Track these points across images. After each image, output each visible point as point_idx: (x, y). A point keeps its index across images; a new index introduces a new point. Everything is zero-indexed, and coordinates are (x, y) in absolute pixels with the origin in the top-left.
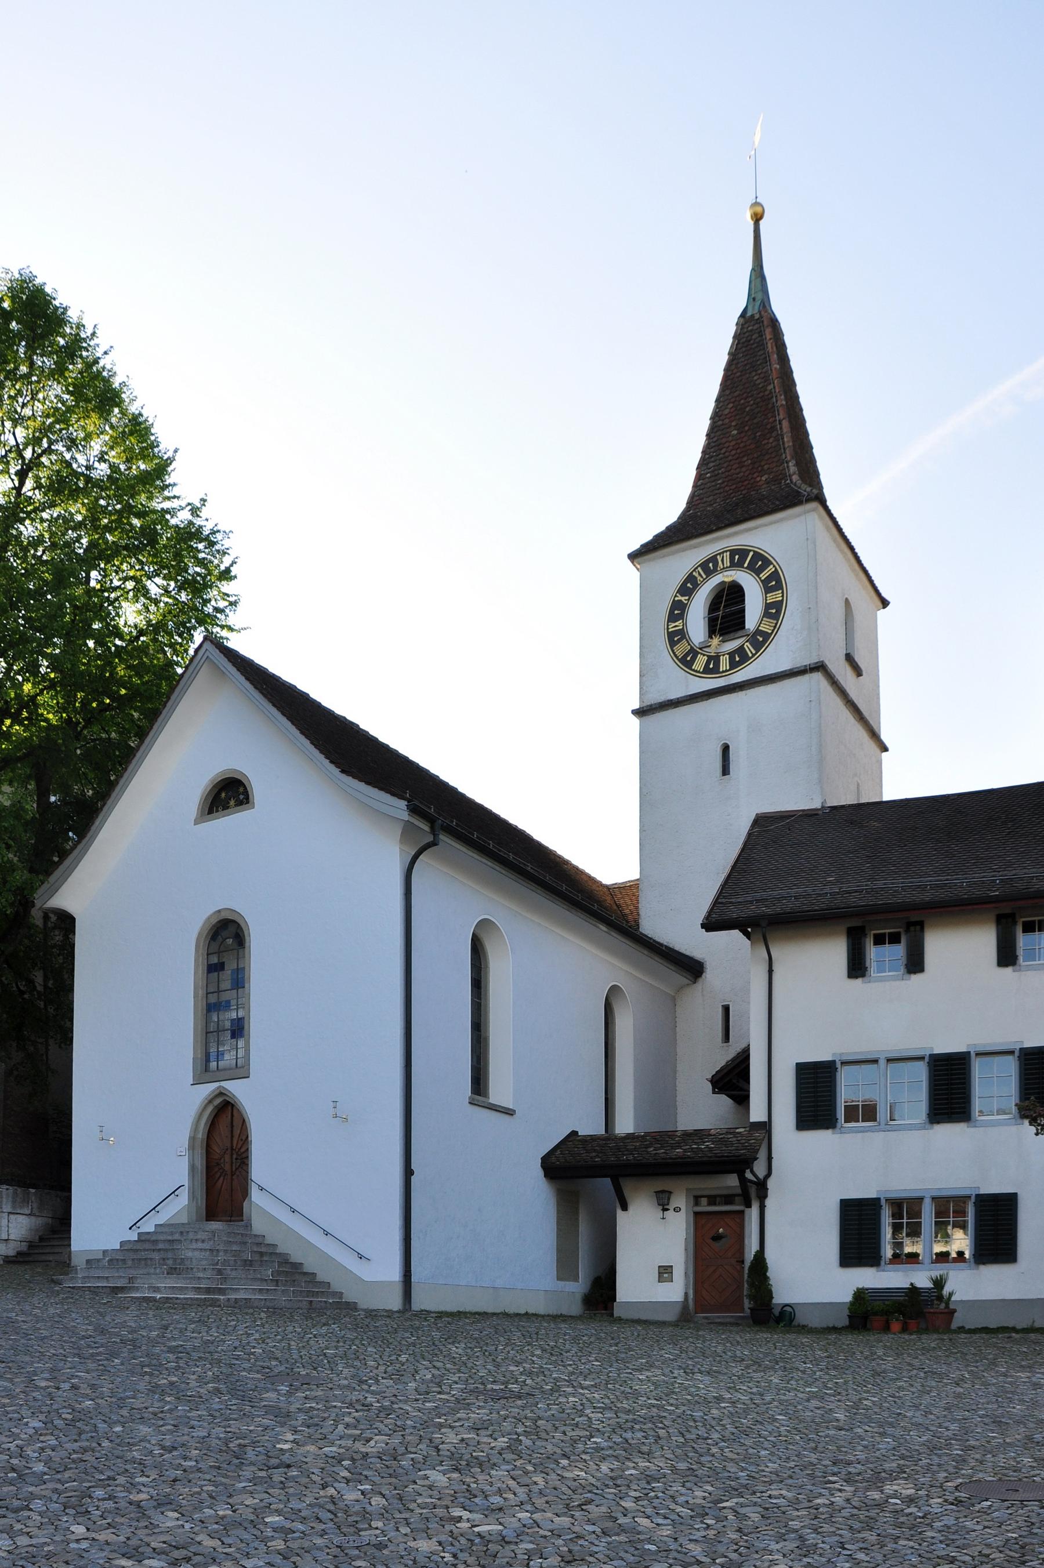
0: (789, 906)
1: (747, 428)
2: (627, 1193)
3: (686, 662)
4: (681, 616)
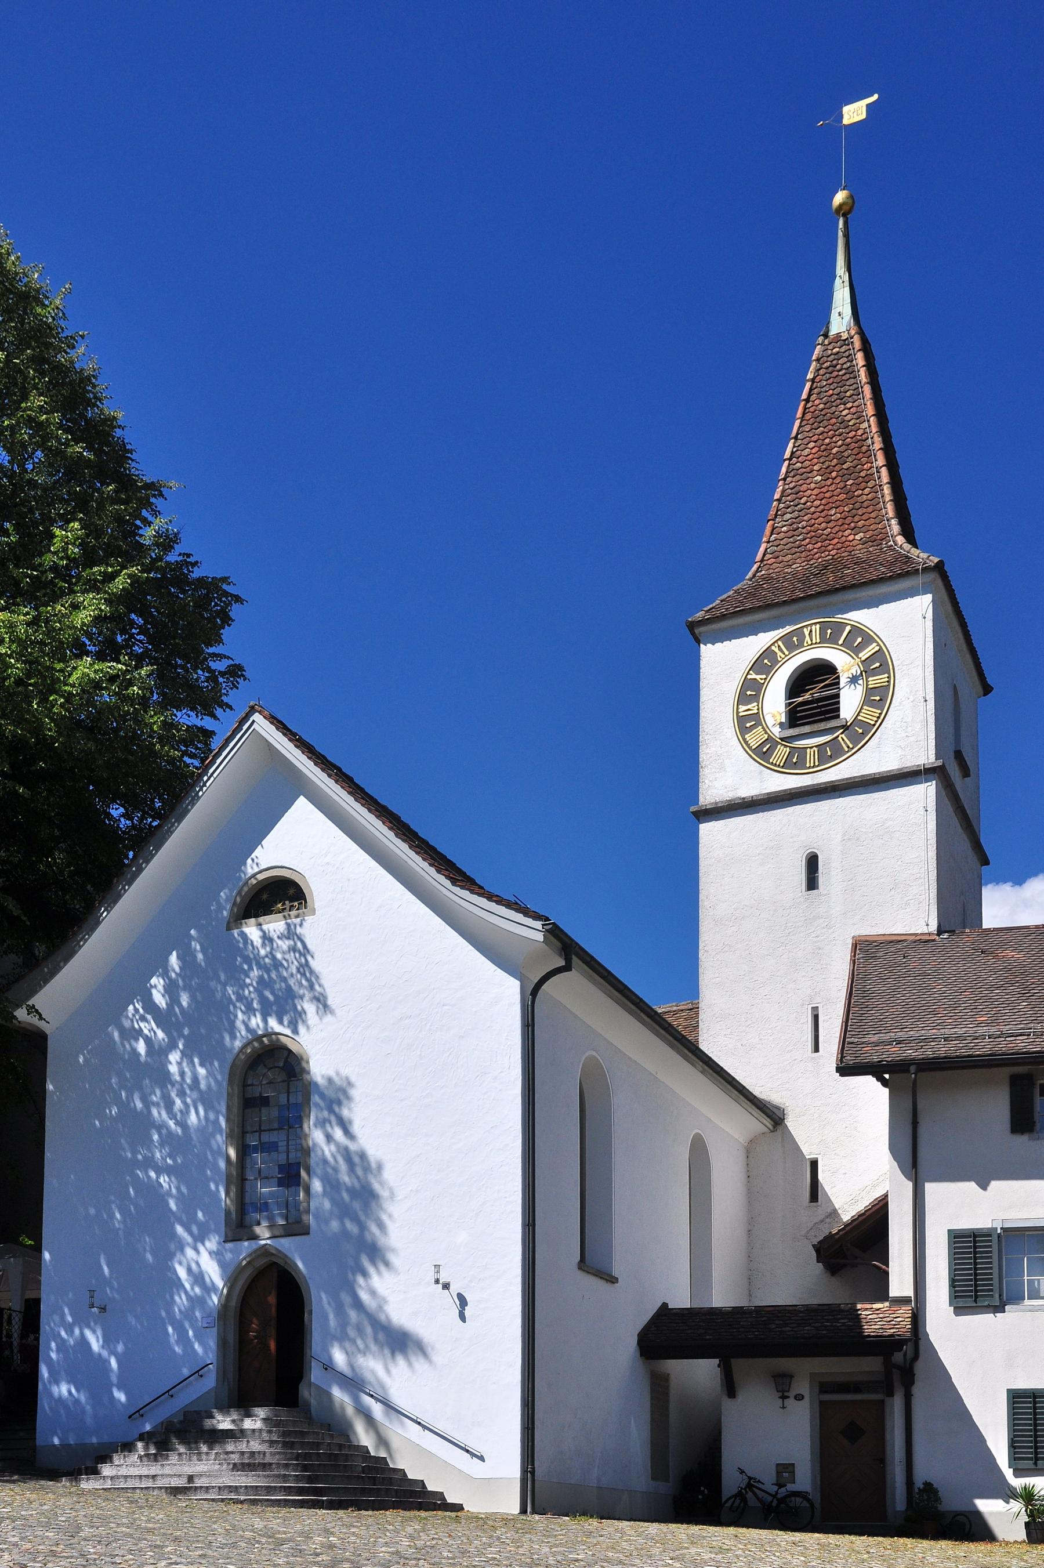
0: (943, 1050)
1: (834, 474)
2: (737, 1376)
3: (762, 753)
4: (756, 698)
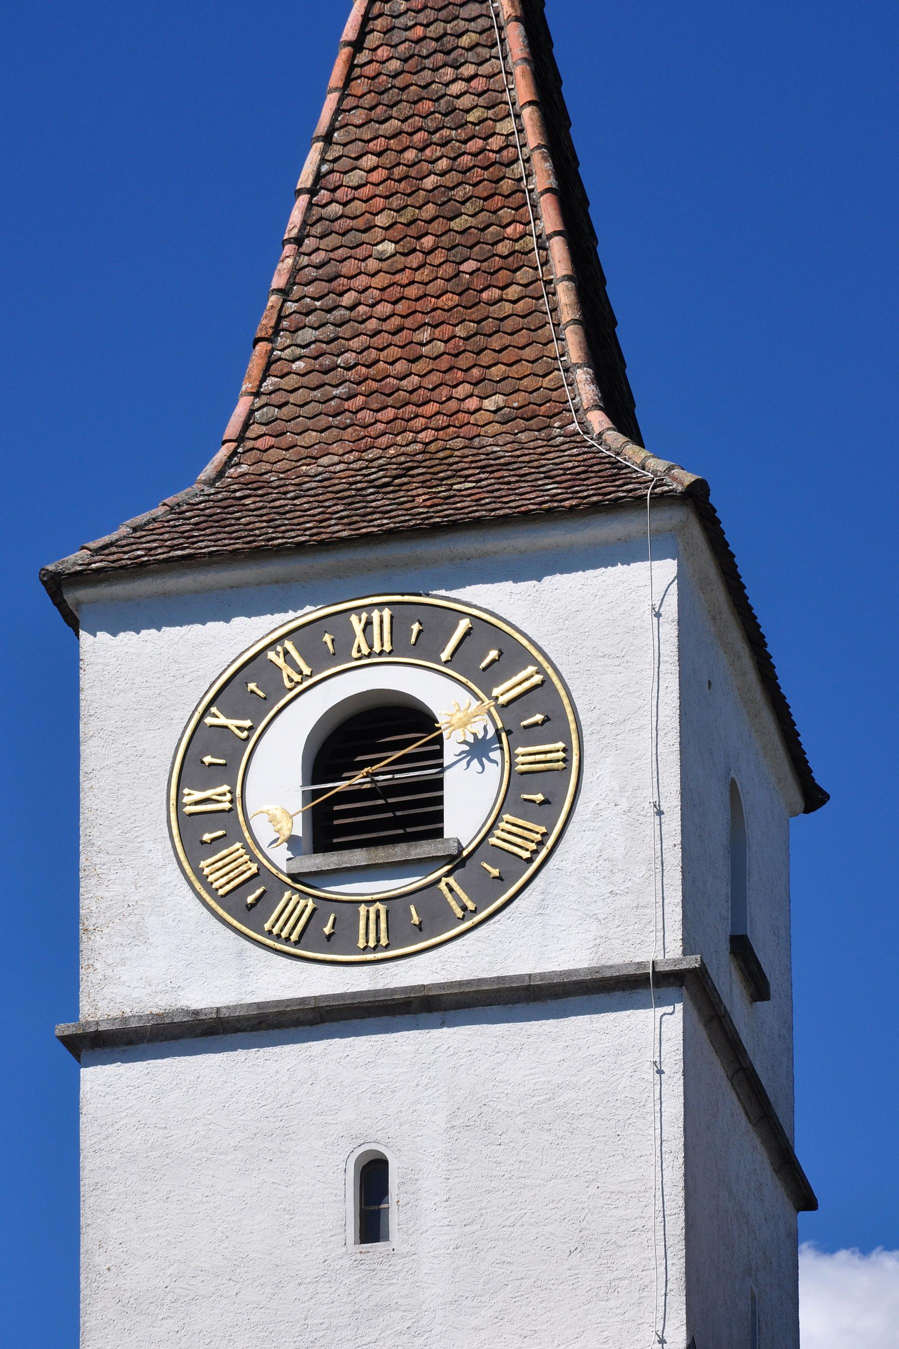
1: (428, 242)
